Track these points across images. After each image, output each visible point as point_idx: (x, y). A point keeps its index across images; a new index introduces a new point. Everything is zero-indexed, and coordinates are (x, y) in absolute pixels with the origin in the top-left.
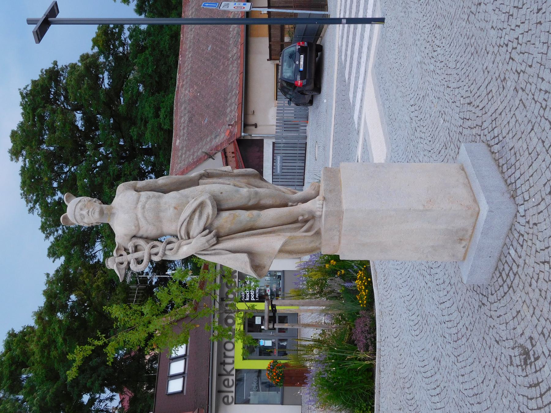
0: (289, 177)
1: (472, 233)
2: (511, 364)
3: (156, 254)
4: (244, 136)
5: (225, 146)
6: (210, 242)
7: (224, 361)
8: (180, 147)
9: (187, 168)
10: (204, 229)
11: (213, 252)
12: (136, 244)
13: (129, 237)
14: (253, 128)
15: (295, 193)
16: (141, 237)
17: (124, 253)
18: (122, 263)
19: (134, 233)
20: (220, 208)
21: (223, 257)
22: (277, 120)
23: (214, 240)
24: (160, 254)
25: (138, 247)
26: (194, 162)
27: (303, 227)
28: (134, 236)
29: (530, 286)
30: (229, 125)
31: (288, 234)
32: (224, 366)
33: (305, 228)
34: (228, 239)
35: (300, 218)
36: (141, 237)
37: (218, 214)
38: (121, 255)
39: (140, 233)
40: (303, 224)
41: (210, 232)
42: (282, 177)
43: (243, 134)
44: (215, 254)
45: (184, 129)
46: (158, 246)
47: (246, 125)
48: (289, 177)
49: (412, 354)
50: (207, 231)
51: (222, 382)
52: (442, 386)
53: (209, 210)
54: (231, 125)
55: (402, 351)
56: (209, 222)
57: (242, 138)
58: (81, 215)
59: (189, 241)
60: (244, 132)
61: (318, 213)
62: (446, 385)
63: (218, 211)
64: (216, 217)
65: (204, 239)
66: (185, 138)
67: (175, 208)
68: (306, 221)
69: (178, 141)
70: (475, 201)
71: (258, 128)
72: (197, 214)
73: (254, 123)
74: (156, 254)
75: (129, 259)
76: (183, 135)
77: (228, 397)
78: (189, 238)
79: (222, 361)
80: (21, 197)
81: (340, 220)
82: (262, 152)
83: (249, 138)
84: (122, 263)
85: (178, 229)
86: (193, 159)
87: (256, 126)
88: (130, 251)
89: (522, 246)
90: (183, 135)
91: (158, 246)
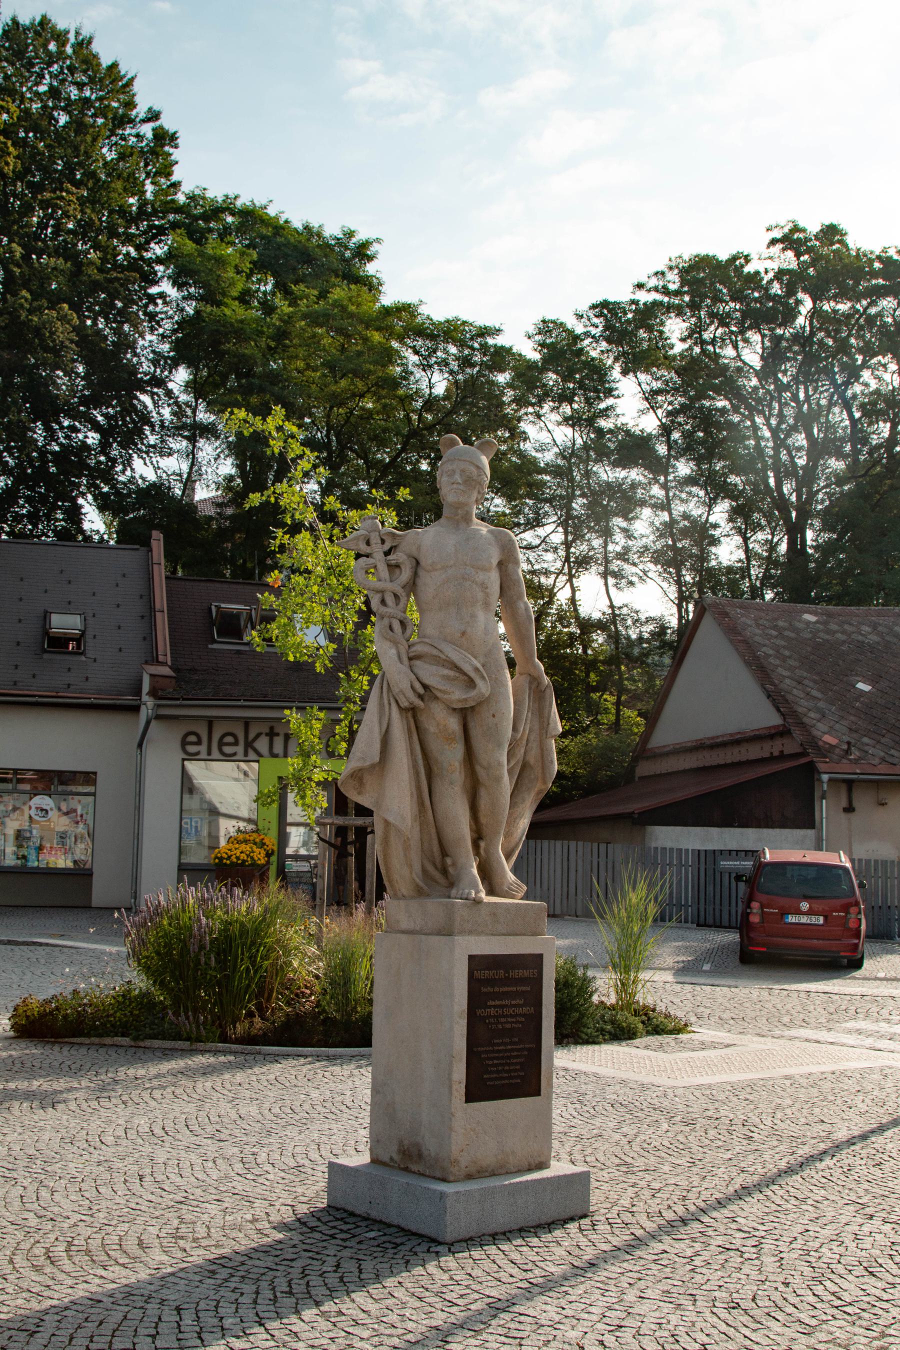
0: (710, 888)
1: (414, 1172)
2: (181, 1222)
3: (383, 602)
4: (820, 780)
5: (797, 733)
6: (401, 696)
7: (278, 735)
8: (798, 624)
9: (745, 642)
10: (425, 687)
11: (386, 702)
12: (403, 567)
13: (415, 554)
14: (844, 803)
15: (508, 857)
16: (415, 575)
17: (387, 547)
18: (368, 543)
19: (423, 563)
20: (465, 714)
21: (376, 719)
22: (868, 862)
23: (405, 704)
24: (383, 609)
25: (397, 571)
26: (757, 658)
27: (436, 868)
28: (418, 563)
29: (305, 1250)
30: (849, 743)
31: (415, 835)
32: (267, 735)
33: (430, 868)
34: (409, 730)
35: (449, 861)
36: (415, 575)
37: (454, 709)
38: (383, 542)
39: (421, 573)
40: (439, 866)
41: (421, 697)
42: (710, 873)
43: (825, 777)
44: (381, 705)
45: (844, 632)
46: (397, 604)
47: (850, 784)
48: (710, 888)
49: (237, 1101)
50: (421, 690)
51: (230, 730)
52: (166, 1138)
53: (458, 695)
54: (849, 748)
55: (247, 1086)
56: (439, 694)
57: (816, 776)
58: (454, 471)
59: (405, 659)
60: (830, 780)
61: (454, 892)
62: (167, 1144)
63: (462, 709)
64: (448, 707)
65: (405, 685)
66: (821, 634)
67: (464, 634)
68: (444, 871)
69: (812, 618)
70: (469, 1177)
71: (843, 815)
72: (451, 673)
73: (855, 804)
74: (383, 602)
75: (375, 555)
76: (828, 632)
77: (199, 743)
78: (410, 659)
79: (276, 731)
80: (532, 330)
81: (439, 933)
82: (783, 826)
83: (817, 794)
84: (368, 543)
85: (427, 640)
86: (768, 656)
87: (849, 809)
88: (389, 558)
89: (378, 1246)
90: (828, 632)
91: (397, 604)
